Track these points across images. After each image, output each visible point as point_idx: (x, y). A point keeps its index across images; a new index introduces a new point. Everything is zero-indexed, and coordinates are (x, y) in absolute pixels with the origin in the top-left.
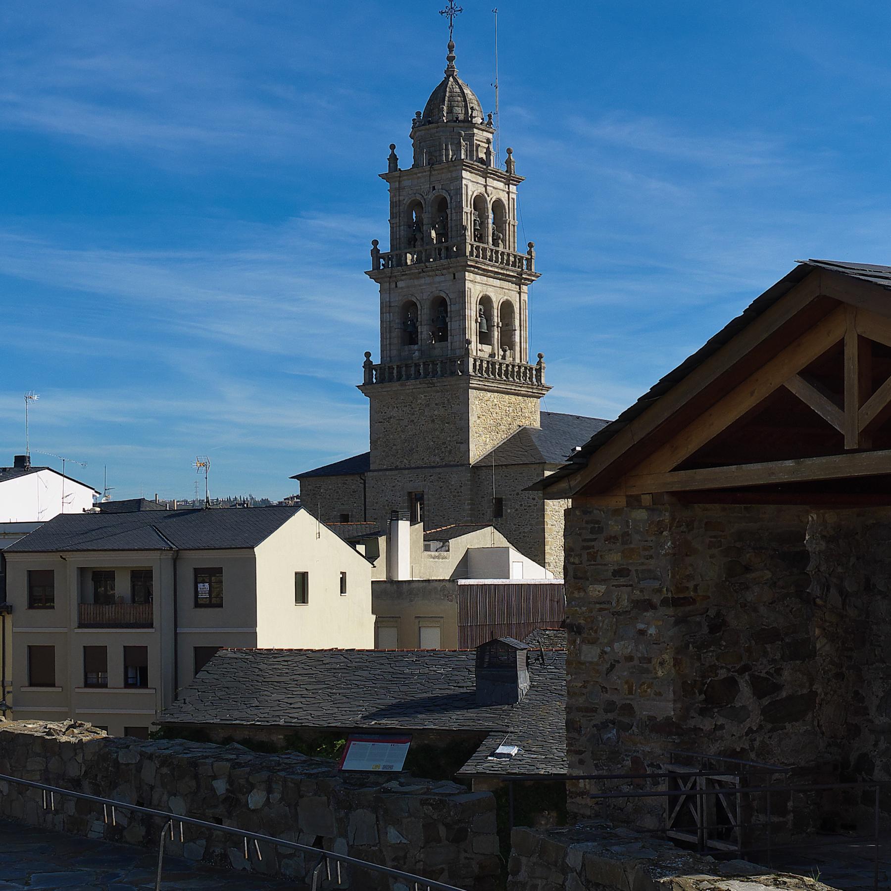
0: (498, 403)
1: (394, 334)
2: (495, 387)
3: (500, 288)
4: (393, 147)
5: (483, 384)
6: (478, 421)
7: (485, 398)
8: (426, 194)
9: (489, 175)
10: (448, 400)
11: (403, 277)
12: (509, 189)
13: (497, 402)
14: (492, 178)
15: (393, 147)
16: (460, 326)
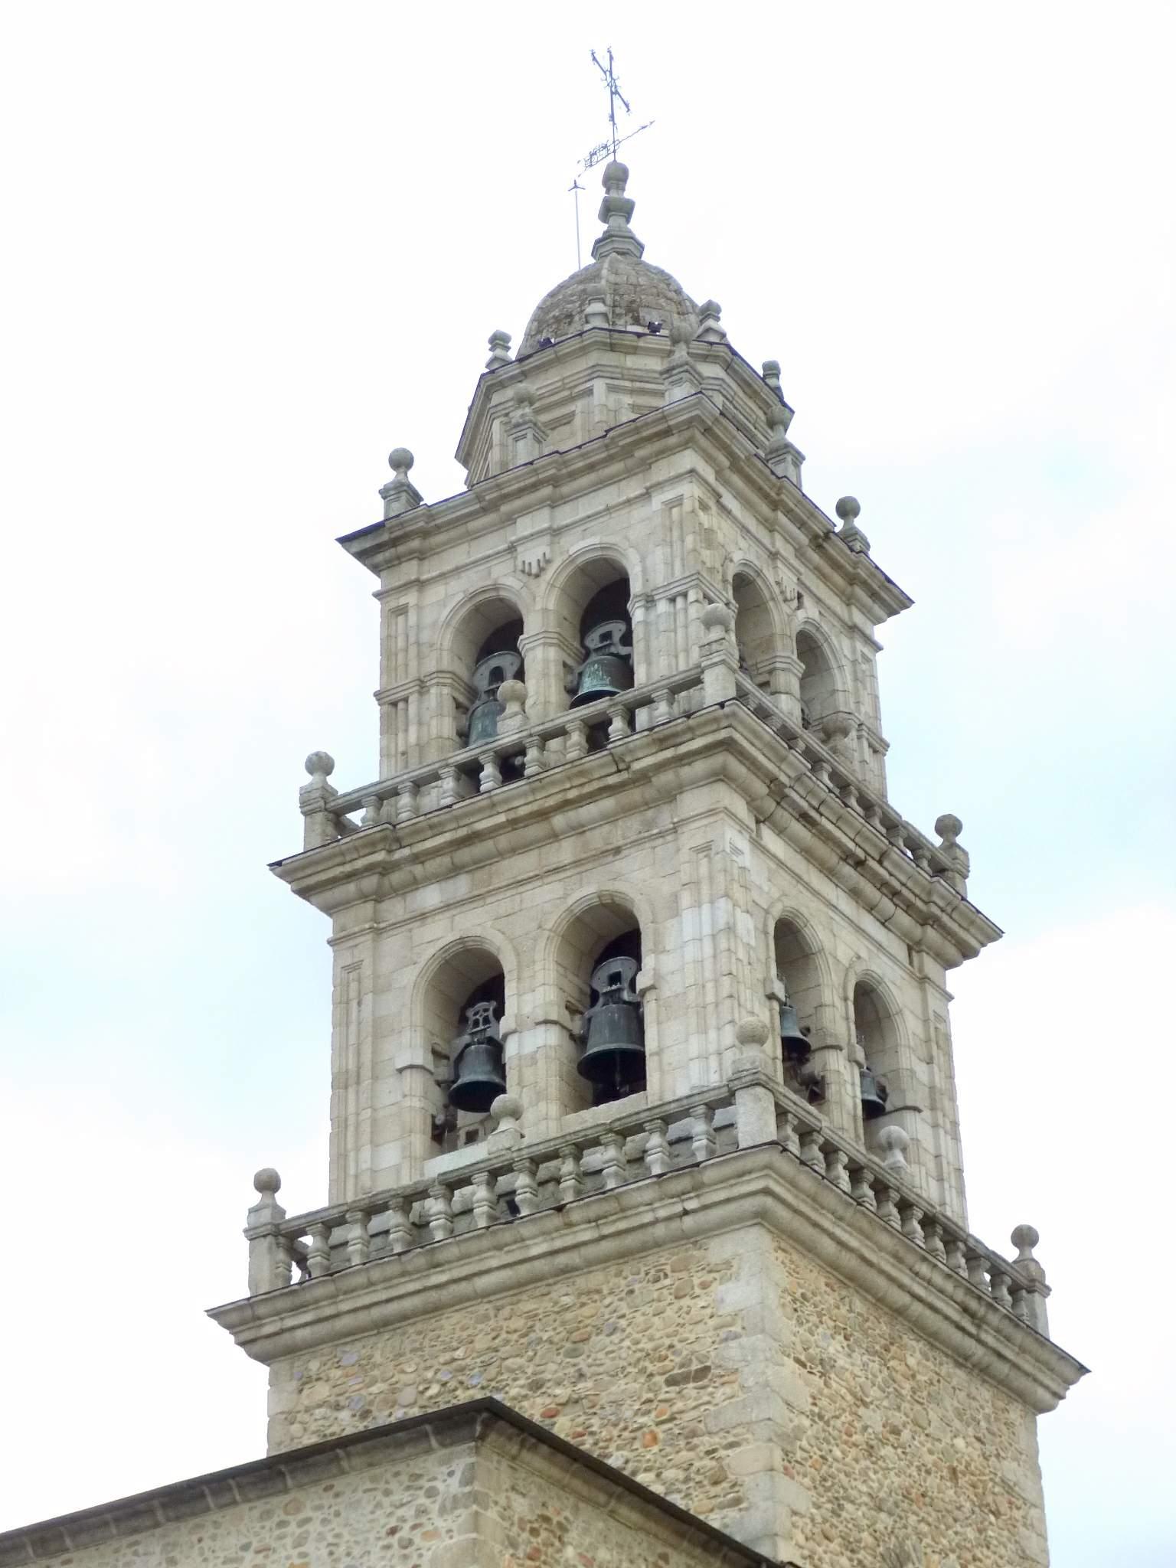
11: (797, 828)
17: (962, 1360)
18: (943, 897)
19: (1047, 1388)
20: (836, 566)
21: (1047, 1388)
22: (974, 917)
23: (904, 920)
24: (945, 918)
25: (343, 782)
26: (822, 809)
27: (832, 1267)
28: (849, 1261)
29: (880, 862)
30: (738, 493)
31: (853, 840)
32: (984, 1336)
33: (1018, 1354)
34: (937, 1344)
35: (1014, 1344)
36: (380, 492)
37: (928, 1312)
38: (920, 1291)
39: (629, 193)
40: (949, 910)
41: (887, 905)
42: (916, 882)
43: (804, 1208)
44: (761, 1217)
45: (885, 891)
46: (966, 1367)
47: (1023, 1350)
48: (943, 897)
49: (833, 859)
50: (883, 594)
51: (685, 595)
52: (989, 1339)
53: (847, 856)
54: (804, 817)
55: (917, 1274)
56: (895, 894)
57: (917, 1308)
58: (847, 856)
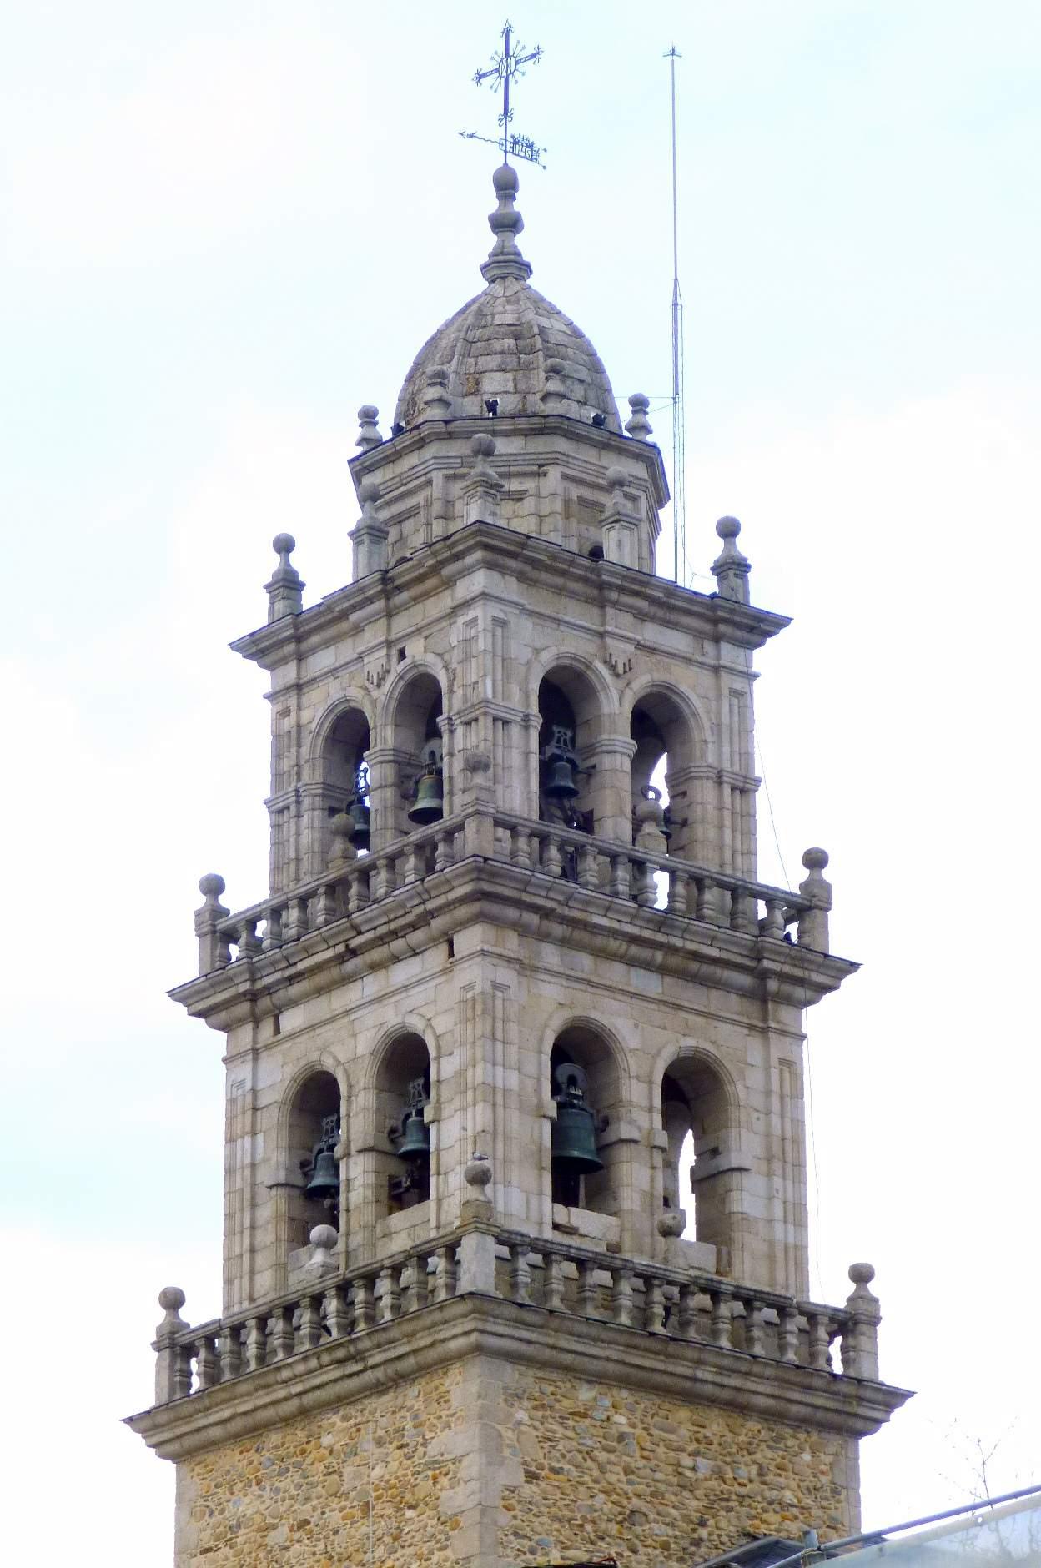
0: (638, 1431)
1: (265, 1213)
2: (608, 1359)
3: (666, 1003)
4: (285, 546)
5: (550, 1341)
6: (528, 1490)
7: (566, 1403)
8: (375, 681)
9: (614, 596)
10: (416, 1417)
11: (295, 990)
12: (718, 657)
13: (633, 1426)
14: (628, 608)
15: (285, 546)
16: (465, 1129)
17: (379, 1388)
18: (411, 898)
19: (455, 1337)
20: (420, 579)
21: (455, 1337)
22: (442, 878)
23: (417, 937)
24: (430, 905)
25: (236, 901)
26: (291, 961)
27: (237, 1437)
28: (237, 1425)
29: (360, 933)
30: (325, 643)
31: (329, 948)
32: (371, 1362)
33: (409, 1342)
34: (352, 1399)
35: (399, 1340)
36: (713, 569)
37: (318, 1393)
38: (298, 1388)
39: (518, 206)
40: (426, 896)
41: (397, 945)
42: (391, 910)
43: (178, 1431)
44: (479, 1349)
45: (387, 940)
46: (391, 1387)
47: (412, 1335)
48: (411, 898)
49: (335, 972)
50: (456, 550)
51: (288, 808)
52: (378, 1358)
53: (341, 959)
54: (291, 980)
55: (284, 1382)
56: (395, 934)
57: (308, 1399)
58: (341, 959)
